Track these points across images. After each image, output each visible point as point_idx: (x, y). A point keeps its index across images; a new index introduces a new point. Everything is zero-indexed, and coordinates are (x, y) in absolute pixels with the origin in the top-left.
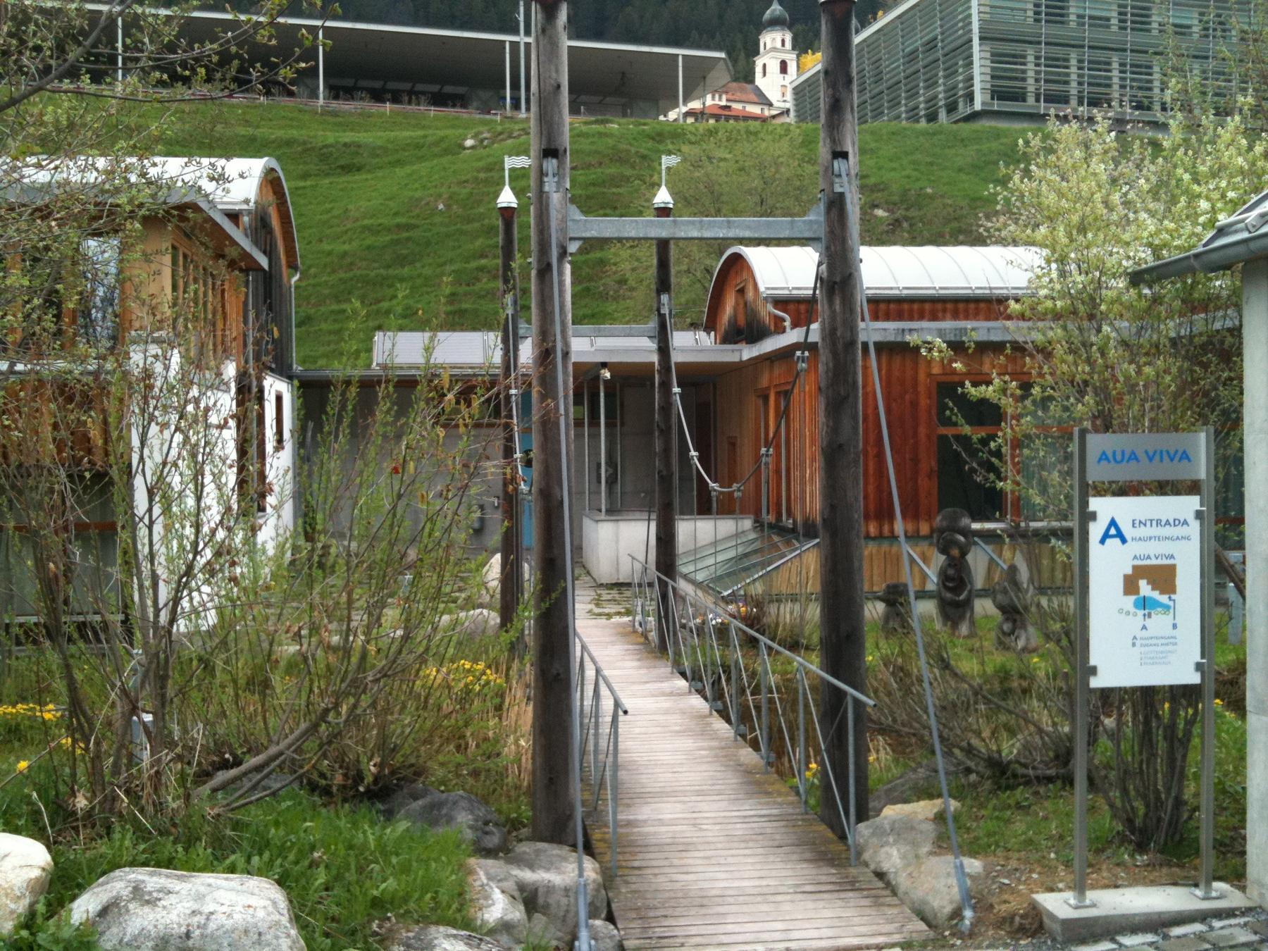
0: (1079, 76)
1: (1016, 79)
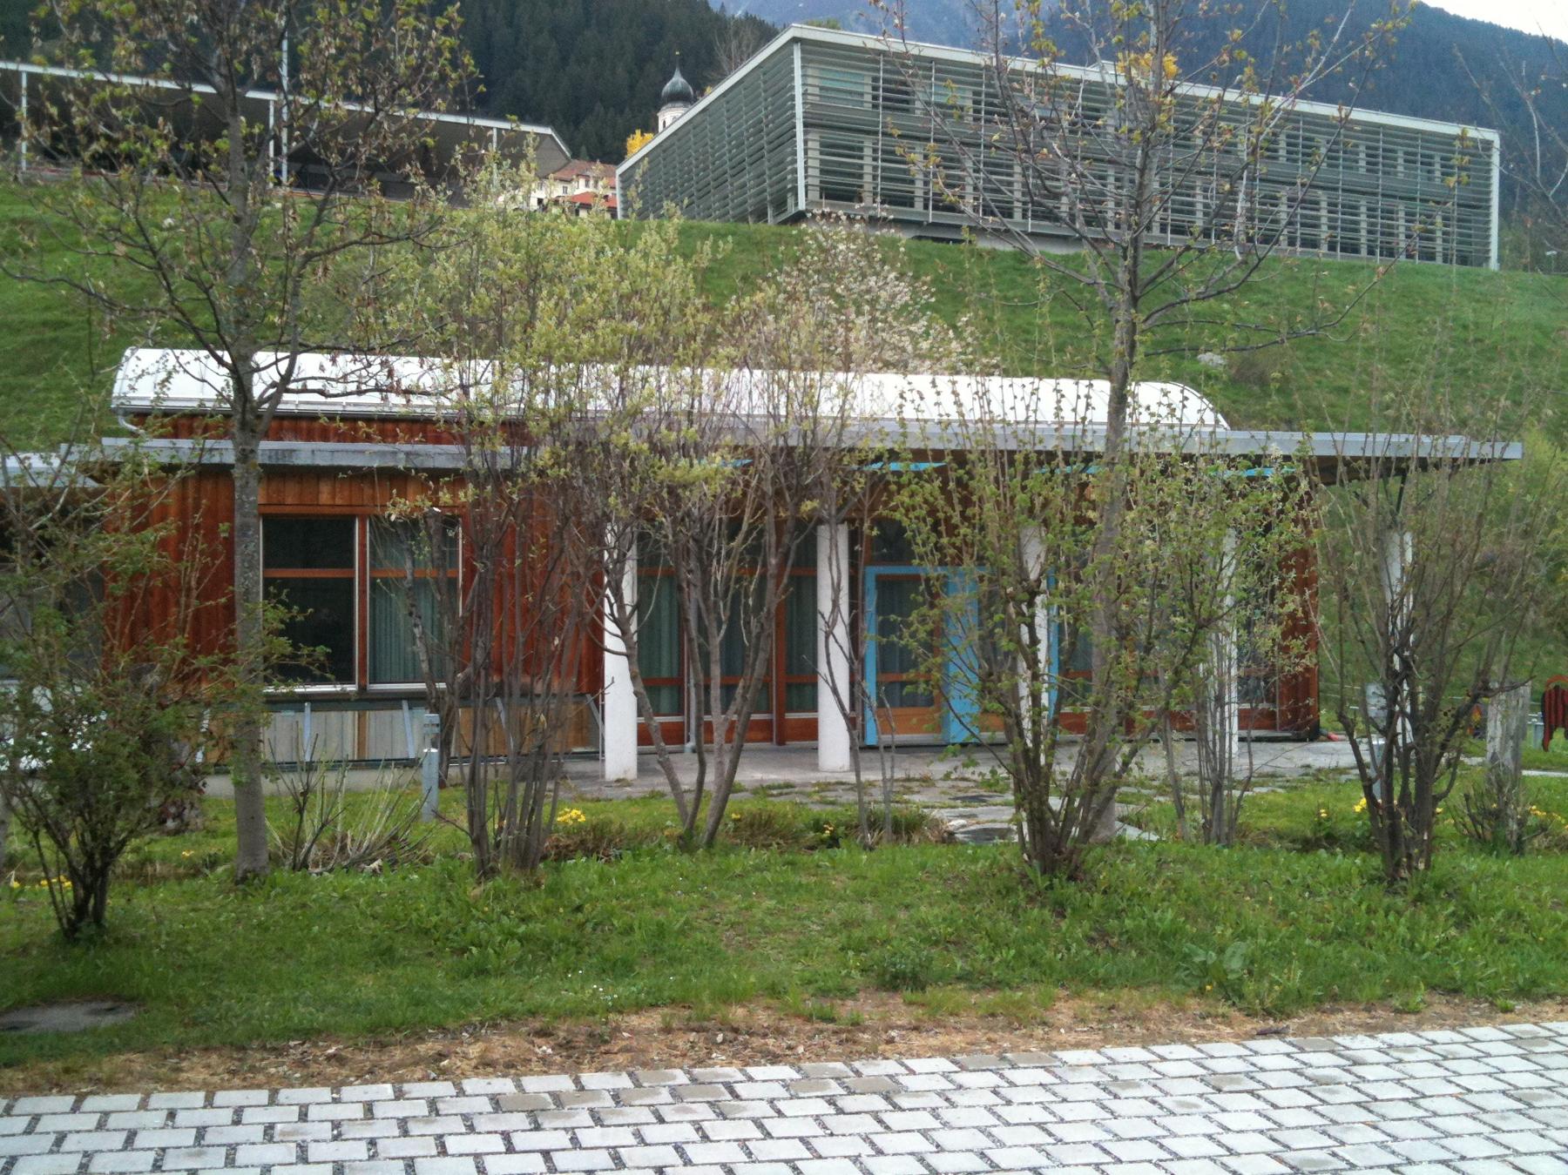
0: (1330, 220)
1: (903, 181)
